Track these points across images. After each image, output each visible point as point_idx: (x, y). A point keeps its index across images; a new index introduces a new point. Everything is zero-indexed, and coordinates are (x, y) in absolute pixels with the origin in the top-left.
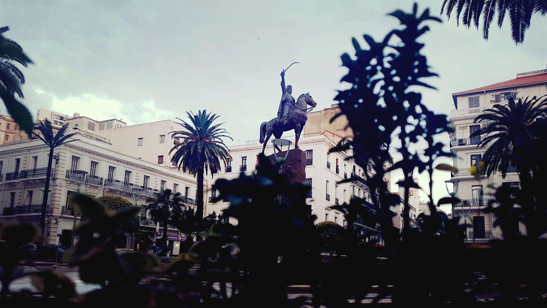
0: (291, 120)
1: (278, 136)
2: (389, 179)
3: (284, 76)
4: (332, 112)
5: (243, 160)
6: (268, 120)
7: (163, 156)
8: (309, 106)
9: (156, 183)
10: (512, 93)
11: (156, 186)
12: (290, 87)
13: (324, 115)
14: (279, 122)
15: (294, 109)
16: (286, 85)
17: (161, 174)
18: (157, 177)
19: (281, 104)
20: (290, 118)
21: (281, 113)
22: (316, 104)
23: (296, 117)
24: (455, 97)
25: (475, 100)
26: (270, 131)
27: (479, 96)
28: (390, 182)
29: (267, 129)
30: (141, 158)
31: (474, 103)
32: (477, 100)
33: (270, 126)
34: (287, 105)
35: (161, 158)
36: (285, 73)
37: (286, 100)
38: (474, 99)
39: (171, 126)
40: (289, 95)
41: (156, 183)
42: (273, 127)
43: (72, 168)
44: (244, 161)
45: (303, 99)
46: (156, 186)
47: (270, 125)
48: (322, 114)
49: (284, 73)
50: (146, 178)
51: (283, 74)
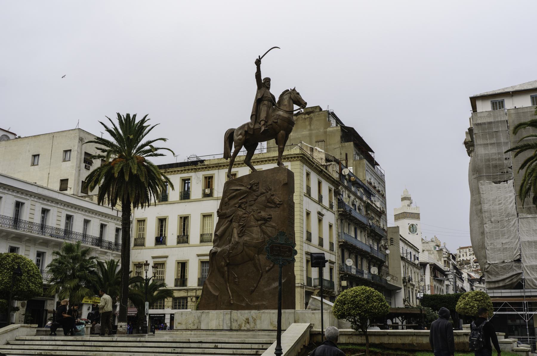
0: (271, 126)
1: (251, 149)
2: (385, 210)
3: (260, 64)
4: (306, 117)
5: (185, 183)
6: (236, 126)
7: (67, 180)
9: (59, 218)
11: (59, 222)
12: (268, 80)
14: (254, 129)
15: (274, 110)
18: (60, 210)
19: (256, 103)
20: (270, 122)
21: (255, 115)
23: (278, 122)
24: (474, 100)
25: (499, 104)
26: (239, 141)
27: (504, 100)
28: (385, 213)
29: (236, 138)
30: (36, 183)
33: (241, 134)
34: (265, 104)
35: (64, 183)
36: (262, 60)
37: (263, 97)
39: (81, 137)
40: (267, 90)
41: (59, 218)
42: (244, 135)
43: (404, 275)
44: (186, 184)
45: (286, 97)
46: (59, 222)
47: (239, 133)
51: (258, 62)
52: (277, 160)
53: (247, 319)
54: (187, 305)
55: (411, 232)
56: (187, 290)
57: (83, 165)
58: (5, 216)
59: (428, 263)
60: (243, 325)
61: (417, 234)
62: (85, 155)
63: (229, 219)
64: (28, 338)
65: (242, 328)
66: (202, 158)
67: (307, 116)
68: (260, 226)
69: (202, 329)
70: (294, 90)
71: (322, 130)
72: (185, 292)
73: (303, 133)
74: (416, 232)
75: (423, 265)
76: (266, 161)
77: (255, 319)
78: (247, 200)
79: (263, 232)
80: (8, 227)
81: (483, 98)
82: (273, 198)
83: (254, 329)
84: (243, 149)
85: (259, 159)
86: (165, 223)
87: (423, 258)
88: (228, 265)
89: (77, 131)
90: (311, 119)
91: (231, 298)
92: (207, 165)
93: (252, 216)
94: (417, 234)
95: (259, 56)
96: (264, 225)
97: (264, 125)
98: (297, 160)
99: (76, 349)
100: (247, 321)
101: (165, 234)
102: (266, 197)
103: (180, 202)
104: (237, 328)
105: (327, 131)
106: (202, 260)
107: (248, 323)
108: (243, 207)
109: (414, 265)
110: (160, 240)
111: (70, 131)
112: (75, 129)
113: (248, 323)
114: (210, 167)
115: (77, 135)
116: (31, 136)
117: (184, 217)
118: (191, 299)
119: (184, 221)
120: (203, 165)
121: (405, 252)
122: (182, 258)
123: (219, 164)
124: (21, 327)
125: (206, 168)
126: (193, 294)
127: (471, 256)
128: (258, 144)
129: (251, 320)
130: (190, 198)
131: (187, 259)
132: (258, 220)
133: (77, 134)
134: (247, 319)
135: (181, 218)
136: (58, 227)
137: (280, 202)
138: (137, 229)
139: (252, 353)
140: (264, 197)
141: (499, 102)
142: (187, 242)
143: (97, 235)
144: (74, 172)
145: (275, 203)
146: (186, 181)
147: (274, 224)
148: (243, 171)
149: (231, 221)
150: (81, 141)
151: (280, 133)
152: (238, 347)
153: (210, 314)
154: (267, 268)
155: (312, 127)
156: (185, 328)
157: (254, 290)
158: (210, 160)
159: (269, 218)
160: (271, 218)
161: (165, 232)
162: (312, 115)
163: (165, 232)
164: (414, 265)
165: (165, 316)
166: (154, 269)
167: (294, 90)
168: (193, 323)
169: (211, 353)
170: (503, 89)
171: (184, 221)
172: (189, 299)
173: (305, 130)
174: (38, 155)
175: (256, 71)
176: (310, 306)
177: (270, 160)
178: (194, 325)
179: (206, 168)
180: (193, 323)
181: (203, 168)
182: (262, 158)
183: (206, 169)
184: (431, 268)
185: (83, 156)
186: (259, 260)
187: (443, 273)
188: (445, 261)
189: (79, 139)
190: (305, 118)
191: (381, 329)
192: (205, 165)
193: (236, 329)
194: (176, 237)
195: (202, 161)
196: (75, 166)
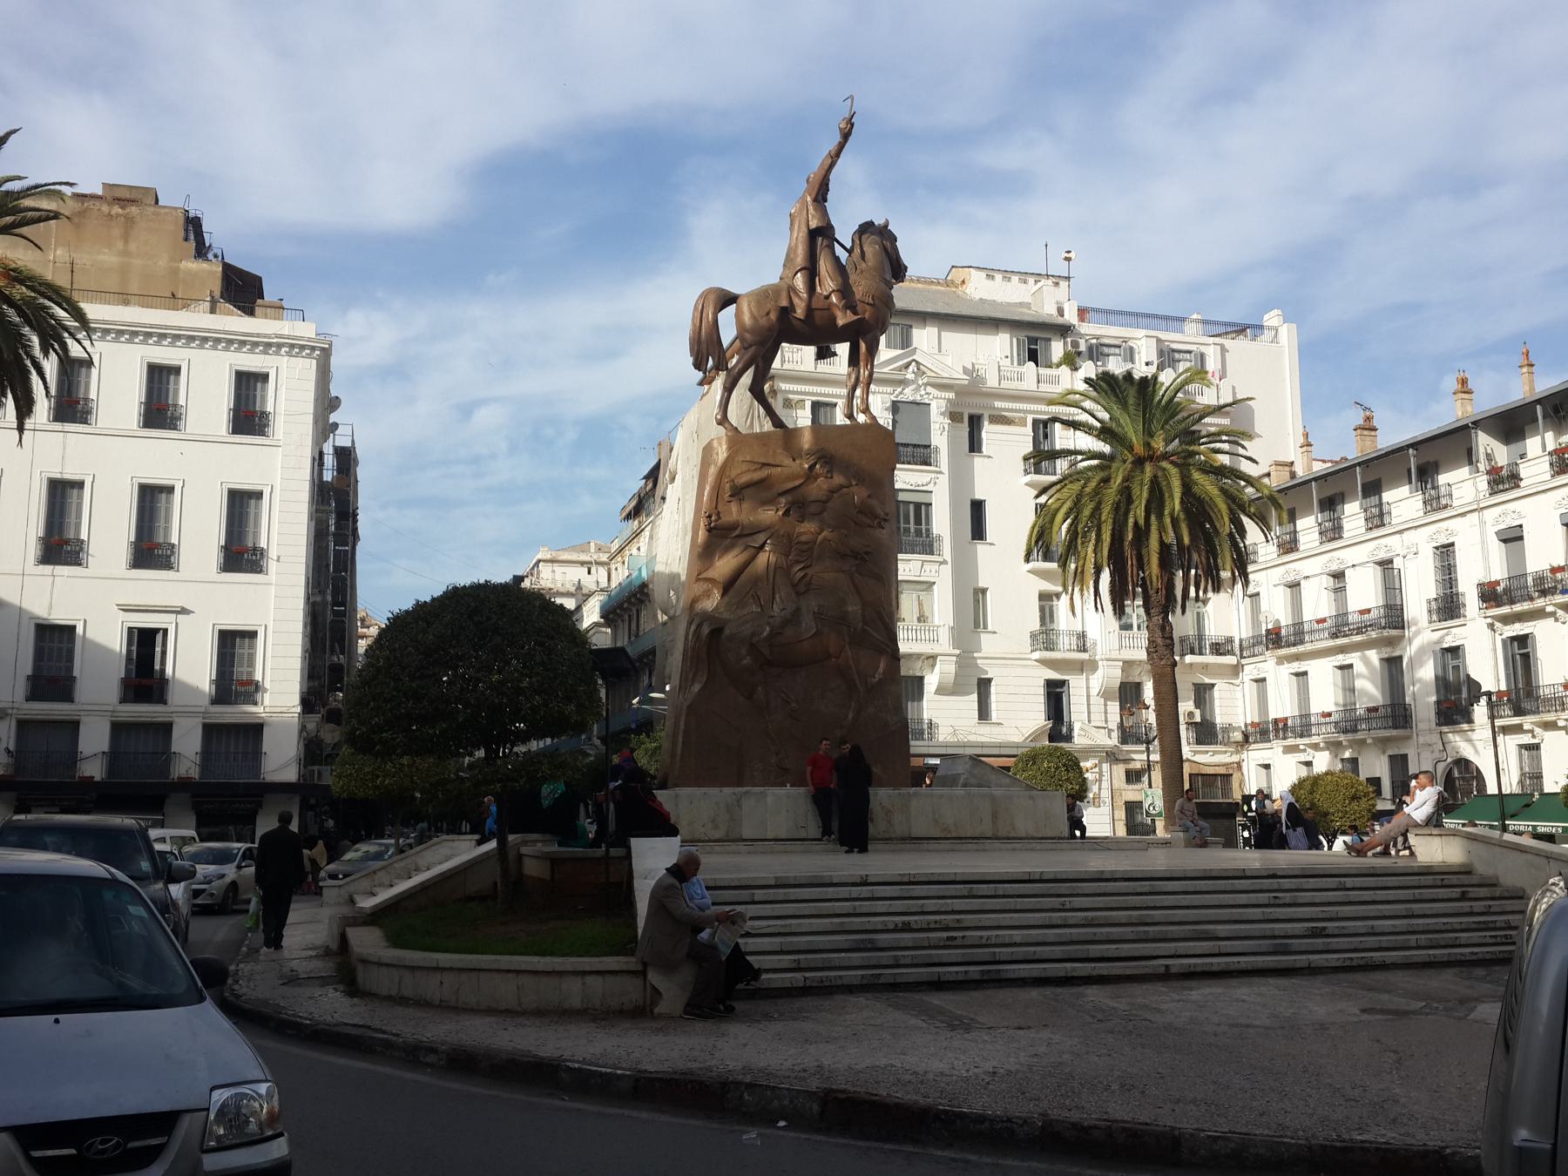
67: (116, 210)
69: (744, 837)
71: (163, 262)
73: (101, 257)
77: (889, 811)
83: (887, 836)
90: (130, 221)
105: (178, 268)
122: (235, 621)
153: (770, 799)
155: (132, 247)
162: (134, 210)
168: (713, 821)
169: (1365, 902)
173: (107, 251)
178: (716, 827)
180: (713, 821)
190: (109, 214)
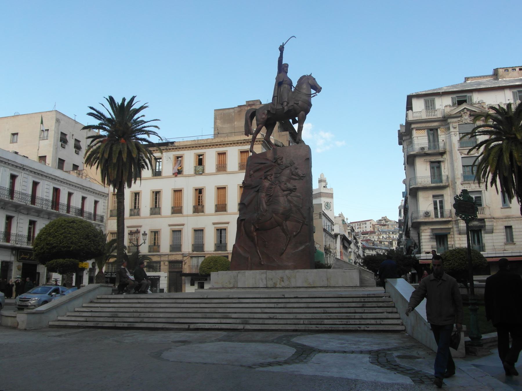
0: (292, 107)
7: (46, 156)
8: (313, 91)
10: (468, 97)
13: (238, 112)
16: (284, 62)
17: (60, 181)
22: (321, 88)
25: (431, 102)
31: (430, 106)
32: (433, 103)
38: (430, 101)
39: (58, 119)
42: (267, 115)
46: (48, 194)
48: (236, 112)
49: (283, 48)
50: (35, 184)
51: (282, 49)
52: (250, 142)
53: (282, 278)
54: (160, 269)
55: (326, 209)
56: (160, 256)
57: (60, 143)
58: (3, 187)
59: (339, 234)
60: (278, 283)
61: (331, 210)
62: (61, 135)
63: (256, 189)
64: (106, 296)
65: (278, 286)
66: (171, 141)
68: (287, 195)
70: (310, 75)
72: (158, 257)
74: (330, 208)
75: (336, 236)
76: (231, 144)
77: (289, 278)
78: (272, 173)
79: (289, 202)
80: (6, 197)
81: (418, 96)
82: (297, 171)
84: (264, 128)
85: (225, 142)
86: (139, 196)
87: (337, 229)
88: (257, 230)
89: (54, 112)
91: (262, 259)
92: (178, 146)
93: (279, 187)
94: (331, 210)
95: (283, 43)
96: (290, 195)
97: (287, 105)
98: (258, 144)
99: (217, 304)
100: (282, 279)
101: (138, 206)
102: (291, 170)
103: (152, 178)
104: (272, 286)
106: (173, 230)
107: (283, 281)
108: (269, 179)
109: (331, 235)
110: (177, 210)
111: (48, 112)
112: (52, 111)
113: (283, 281)
114: (180, 148)
115: (54, 116)
116: (10, 116)
117: (156, 192)
118: (164, 263)
119: (156, 195)
120: (174, 146)
121: (325, 225)
123: (212, 143)
124: (101, 286)
125: (176, 148)
126: (165, 258)
127: (359, 229)
128: (276, 123)
129: (285, 278)
130: (162, 175)
131: (160, 228)
132: (284, 191)
133: (54, 116)
134: (281, 278)
135: (153, 192)
136: (47, 198)
137: (303, 175)
138: (112, 203)
139: (358, 306)
140: (289, 170)
141: (431, 100)
142: (138, 214)
143: (80, 207)
144: (52, 149)
145: (299, 176)
146: (222, 154)
147: (299, 194)
148: (259, 149)
149: (258, 191)
150: (58, 122)
151: (301, 113)
152: (310, 301)
154: (295, 233)
156: (222, 287)
157: (284, 252)
158: (180, 142)
159: (294, 189)
160: (296, 189)
161: (138, 204)
163: (138, 204)
164: (331, 235)
165: (159, 278)
166: (129, 235)
167: (310, 75)
170: (434, 90)
171: (156, 195)
172: (162, 263)
174: (17, 134)
175: (279, 56)
176: (334, 266)
177: (234, 143)
178: (230, 283)
179: (176, 148)
181: (173, 149)
182: (228, 142)
183: (177, 150)
184: (341, 238)
185: (59, 136)
186: (286, 226)
187: (350, 243)
188: (349, 232)
189: (56, 120)
191: (479, 282)
192: (175, 146)
193: (271, 287)
194: (149, 209)
195: (172, 143)
196: (52, 145)
